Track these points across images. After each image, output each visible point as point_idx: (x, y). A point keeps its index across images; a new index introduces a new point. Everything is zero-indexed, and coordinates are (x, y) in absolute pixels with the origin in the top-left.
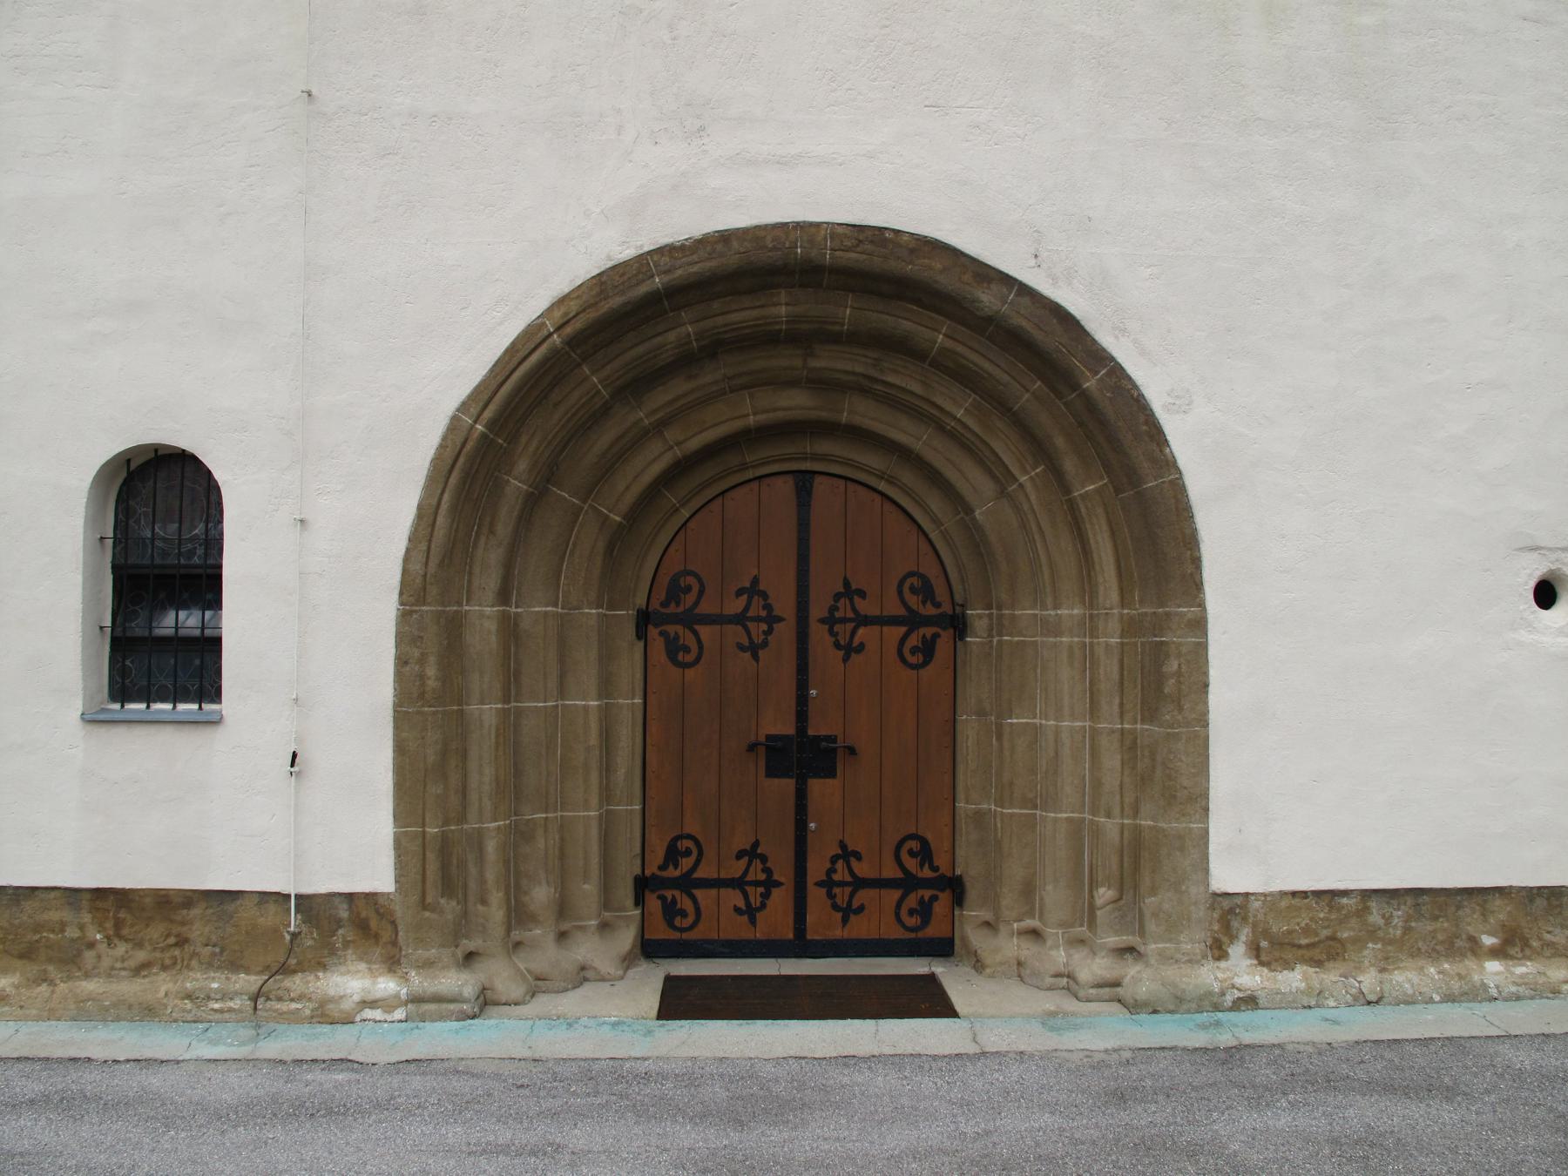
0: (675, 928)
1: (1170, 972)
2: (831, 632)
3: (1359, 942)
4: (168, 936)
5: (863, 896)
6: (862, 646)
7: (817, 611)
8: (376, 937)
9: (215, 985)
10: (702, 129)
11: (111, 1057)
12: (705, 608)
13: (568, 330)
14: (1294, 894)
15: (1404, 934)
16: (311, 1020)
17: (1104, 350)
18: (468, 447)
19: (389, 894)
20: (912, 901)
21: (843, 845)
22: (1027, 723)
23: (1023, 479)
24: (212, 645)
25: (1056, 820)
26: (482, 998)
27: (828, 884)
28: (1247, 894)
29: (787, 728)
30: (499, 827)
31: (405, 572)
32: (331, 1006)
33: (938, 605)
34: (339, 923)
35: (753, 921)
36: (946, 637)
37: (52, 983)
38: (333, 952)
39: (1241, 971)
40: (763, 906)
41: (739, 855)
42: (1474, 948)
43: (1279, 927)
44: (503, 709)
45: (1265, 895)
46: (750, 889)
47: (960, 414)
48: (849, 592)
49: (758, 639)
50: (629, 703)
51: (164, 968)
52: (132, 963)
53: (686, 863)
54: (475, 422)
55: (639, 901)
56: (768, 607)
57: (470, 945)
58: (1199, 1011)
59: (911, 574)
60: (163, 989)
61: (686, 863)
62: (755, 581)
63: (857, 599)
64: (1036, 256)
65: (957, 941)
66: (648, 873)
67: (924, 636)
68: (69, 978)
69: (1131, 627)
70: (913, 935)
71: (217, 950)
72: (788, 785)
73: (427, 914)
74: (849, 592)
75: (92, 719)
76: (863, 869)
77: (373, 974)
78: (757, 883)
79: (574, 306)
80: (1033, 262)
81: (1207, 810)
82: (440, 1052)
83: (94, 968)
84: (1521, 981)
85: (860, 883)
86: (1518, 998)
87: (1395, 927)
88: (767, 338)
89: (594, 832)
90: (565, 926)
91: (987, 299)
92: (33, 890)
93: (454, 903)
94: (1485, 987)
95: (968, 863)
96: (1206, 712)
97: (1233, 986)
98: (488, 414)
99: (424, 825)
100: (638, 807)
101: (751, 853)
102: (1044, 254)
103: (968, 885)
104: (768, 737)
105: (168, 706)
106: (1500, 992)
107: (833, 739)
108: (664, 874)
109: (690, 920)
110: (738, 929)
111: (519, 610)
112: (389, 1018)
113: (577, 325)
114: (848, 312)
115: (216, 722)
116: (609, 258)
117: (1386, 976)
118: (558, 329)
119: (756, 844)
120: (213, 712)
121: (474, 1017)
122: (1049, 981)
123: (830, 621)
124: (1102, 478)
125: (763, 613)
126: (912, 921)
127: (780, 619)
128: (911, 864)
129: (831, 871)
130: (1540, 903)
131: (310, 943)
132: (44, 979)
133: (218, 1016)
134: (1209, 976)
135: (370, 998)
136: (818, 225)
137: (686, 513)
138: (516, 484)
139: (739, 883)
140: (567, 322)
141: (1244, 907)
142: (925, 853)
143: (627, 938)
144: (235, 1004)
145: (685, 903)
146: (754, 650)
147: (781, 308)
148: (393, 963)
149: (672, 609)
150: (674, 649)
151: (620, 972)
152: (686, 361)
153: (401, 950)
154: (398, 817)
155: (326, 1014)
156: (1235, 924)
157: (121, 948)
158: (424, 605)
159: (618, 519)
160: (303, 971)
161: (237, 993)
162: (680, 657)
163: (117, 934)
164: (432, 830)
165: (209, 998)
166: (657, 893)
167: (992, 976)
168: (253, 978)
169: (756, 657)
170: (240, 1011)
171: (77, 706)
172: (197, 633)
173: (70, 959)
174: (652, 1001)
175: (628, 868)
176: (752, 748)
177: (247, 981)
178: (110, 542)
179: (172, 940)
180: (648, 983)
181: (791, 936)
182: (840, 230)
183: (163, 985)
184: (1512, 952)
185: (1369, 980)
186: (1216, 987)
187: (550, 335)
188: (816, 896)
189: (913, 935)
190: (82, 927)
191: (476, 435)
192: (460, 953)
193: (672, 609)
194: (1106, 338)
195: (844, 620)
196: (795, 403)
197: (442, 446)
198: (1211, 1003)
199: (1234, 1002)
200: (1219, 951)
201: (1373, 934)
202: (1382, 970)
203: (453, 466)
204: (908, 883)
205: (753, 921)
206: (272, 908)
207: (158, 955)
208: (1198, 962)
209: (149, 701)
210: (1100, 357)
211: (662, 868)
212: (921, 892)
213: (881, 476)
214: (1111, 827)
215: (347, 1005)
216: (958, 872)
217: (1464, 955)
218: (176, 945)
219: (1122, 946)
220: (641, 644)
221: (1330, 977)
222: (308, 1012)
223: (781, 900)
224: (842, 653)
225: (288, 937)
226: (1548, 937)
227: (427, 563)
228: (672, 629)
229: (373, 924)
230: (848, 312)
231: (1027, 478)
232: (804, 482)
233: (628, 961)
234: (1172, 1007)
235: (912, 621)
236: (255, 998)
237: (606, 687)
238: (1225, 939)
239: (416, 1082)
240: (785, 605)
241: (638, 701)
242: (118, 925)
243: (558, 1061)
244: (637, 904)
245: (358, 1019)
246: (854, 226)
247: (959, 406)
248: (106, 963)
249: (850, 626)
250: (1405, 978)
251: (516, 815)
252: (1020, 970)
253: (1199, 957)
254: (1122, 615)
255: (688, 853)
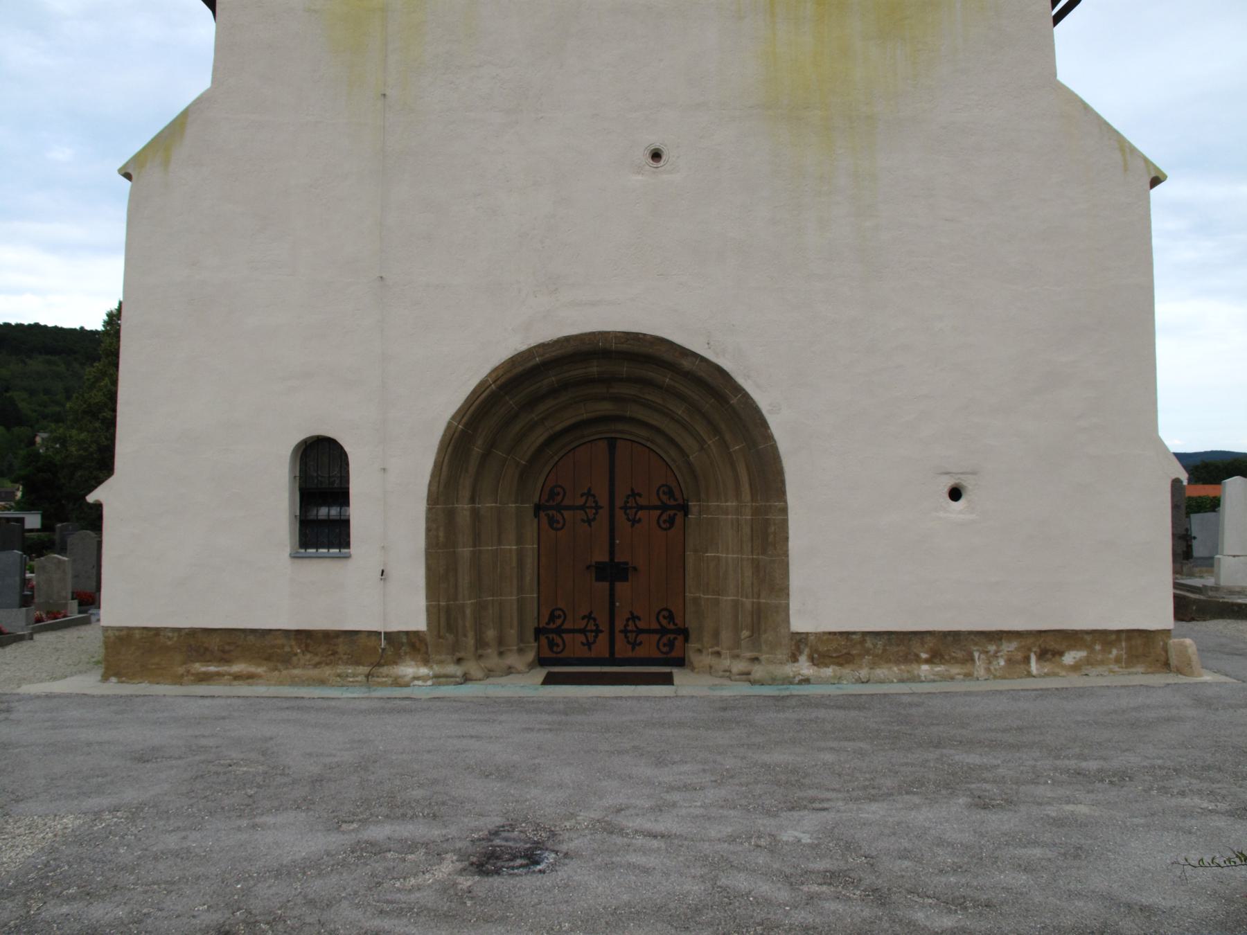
0: (552, 651)
1: (771, 668)
2: (625, 513)
3: (861, 656)
4: (328, 650)
5: (642, 637)
6: (640, 520)
7: (619, 503)
8: (419, 650)
9: (350, 671)
10: (557, 289)
11: (312, 696)
12: (567, 502)
13: (498, 382)
14: (830, 633)
15: (883, 653)
16: (391, 685)
17: (740, 386)
18: (456, 435)
19: (424, 632)
20: (665, 639)
21: (632, 613)
22: (715, 556)
23: (710, 442)
24: (345, 523)
25: (726, 600)
26: (465, 677)
27: (625, 631)
28: (807, 633)
29: (605, 558)
30: (472, 603)
31: (429, 490)
32: (400, 679)
33: (675, 500)
34: (403, 644)
35: (590, 649)
36: (680, 515)
37: (280, 671)
38: (400, 657)
39: (804, 667)
40: (595, 642)
41: (583, 618)
42: (918, 660)
43: (823, 648)
44: (473, 551)
45: (816, 634)
46: (588, 634)
47: (680, 413)
48: (634, 494)
49: (591, 517)
50: (531, 547)
51: (327, 664)
52: (313, 662)
53: (559, 622)
54: (458, 424)
55: (537, 639)
56: (596, 502)
57: (459, 655)
58: (783, 684)
59: (663, 485)
60: (327, 673)
61: (559, 622)
62: (590, 489)
63: (637, 498)
64: (708, 344)
65: (686, 659)
66: (541, 626)
67: (670, 515)
68: (287, 668)
69: (756, 511)
70: (665, 656)
71: (350, 656)
72: (606, 585)
73: (441, 640)
74: (634, 494)
75: (294, 557)
76: (641, 625)
77: (418, 667)
78: (592, 631)
79: (501, 372)
80: (707, 346)
81: (788, 595)
82: (447, 695)
83: (297, 664)
84: (937, 674)
85: (640, 631)
86: (934, 681)
87: (879, 649)
88: (589, 381)
89: (515, 607)
90: (502, 650)
91: (686, 364)
92: (270, 631)
93: (452, 636)
94: (919, 676)
95: (691, 623)
96: (787, 551)
97: (799, 674)
98: (464, 420)
99: (439, 601)
100: (535, 595)
101: (589, 617)
102: (712, 343)
103: (691, 631)
104: (596, 563)
105: (314, 550)
106: (926, 679)
107: (626, 563)
108: (548, 627)
109: (561, 647)
110: (584, 652)
111: (480, 506)
112: (425, 684)
113: (503, 380)
114: (625, 369)
115: (348, 557)
116: (516, 350)
117: (872, 671)
118: (494, 382)
119: (591, 613)
120: (346, 553)
121: (461, 684)
122: (721, 673)
123: (625, 508)
124: (742, 443)
125: (593, 505)
126: (665, 649)
127: (601, 508)
128: (664, 622)
129: (626, 626)
130: (950, 639)
131: (390, 653)
132: (276, 669)
133: (351, 684)
134: (789, 669)
135: (416, 676)
136: (608, 333)
137: (556, 458)
138: (477, 450)
139: (583, 631)
140: (498, 379)
141: (806, 639)
142: (671, 617)
143: (531, 656)
144: (359, 679)
145: (558, 640)
146: (589, 522)
147: (594, 369)
148: (426, 662)
149: (551, 503)
150: (552, 521)
151: (527, 670)
152: (553, 392)
153: (429, 656)
154: (428, 597)
155: (397, 682)
156: (802, 647)
157: (308, 656)
158: (438, 504)
159: (524, 463)
160: (387, 665)
161: (360, 674)
162: (555, 525)
163: (306, 649)
164: (443, 604)
165: (347, 676)
166: (546, 635)
167: (698, 673)
168: (366, 668)
169: (590, 525)
170: (361, 682)
171: (288, 551)
172: (338, 518)
173: (287, 660)
174: (541, 679)
175: (531, 624)
176: (588, 567)
177: (366, 669)
178: (298, 478)
179: (330, 652)
180: (541, 673)
181: (607, 656)
182: (619, 335)
183: (327, 671)
184: (935, 661)
185: (864, 673)
186: (791, 674)
187: (490, 385)
188: (619, 637)
189: (665, 656)
190: (291, 647)
191: (459, 430)
192: (455, 658)
193: (551, 503)
194: (741, 380)
195: (631, 508)
196: (606, 408)
197: (444, 435)
198: (788, 681)
199: (799, 681)
200: (794, 658)
201: (868, 652)
202: (871, 668)
203: (449, 444)
204: (663, 631)
205: (590, 649)
206: (373, 638)
207: (324, 659)
208: (785, 663)
209: (317, 547)
210: (738, 389)
211: (548, 624)
212: (669, 636)
213: (648, 440)
214: (748, 602)
215: (407, 679)
216: (686, 626)
217: (912, 662)
218: (332, 654)
219: (753, 657)
220: (536, 520)
221: (846, 671)
222: (390, 682)
223: (603, 638)
224: (630, 523)
225: (380, 651)
226: (954, 654)
227: (438, 487)
228: (550, 512)
229: (417, 644)
230: (625, 369)
231: (711, 442)
232: (612, 443)
233: (531, 666)
234: (770, 683)
235: (664, 508)
236: (367, 676)
237: (520, 540)
238: (797, 653)
239: (438, 704)
240: (603, 500)
241: (536, 546)
242: (307, 646)
243: (497, 698)
244: (536, 640)
245: (412, 684)
246: (625, 333)
247: (680, 411)
248: (302, 662)
249: (634, 510)
250: (881, 672)
251: (480, 598)
252: (710, 670)
253: (785, 661)
254: (752, 506)
255: (559, 617)
